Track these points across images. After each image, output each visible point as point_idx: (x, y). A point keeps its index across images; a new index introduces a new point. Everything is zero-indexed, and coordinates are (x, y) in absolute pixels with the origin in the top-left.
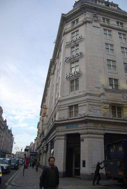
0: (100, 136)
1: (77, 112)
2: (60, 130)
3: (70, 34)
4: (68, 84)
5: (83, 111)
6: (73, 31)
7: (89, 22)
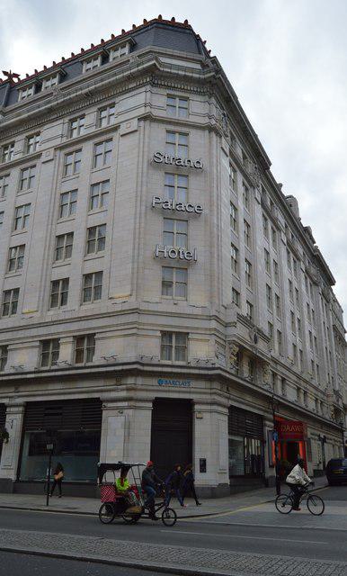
1: (182, 350)
2: (140, 387)
3: (90, 145)
4: (154, 275)
5: (201, 351)
6: (97, 140)
7: (218, 133)
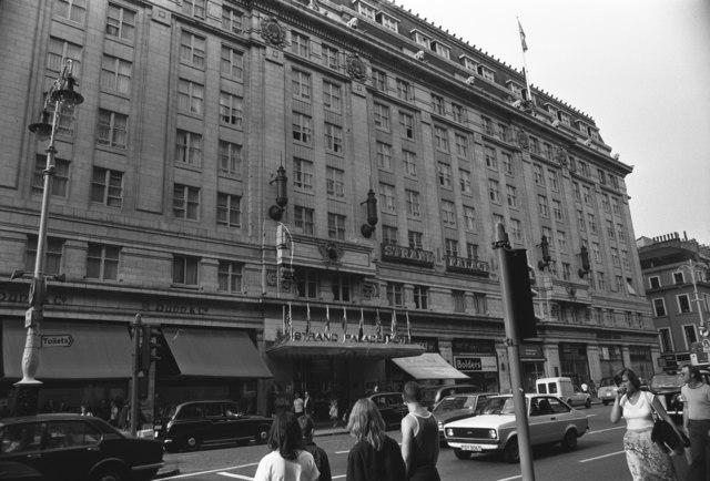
7: (258, 46)
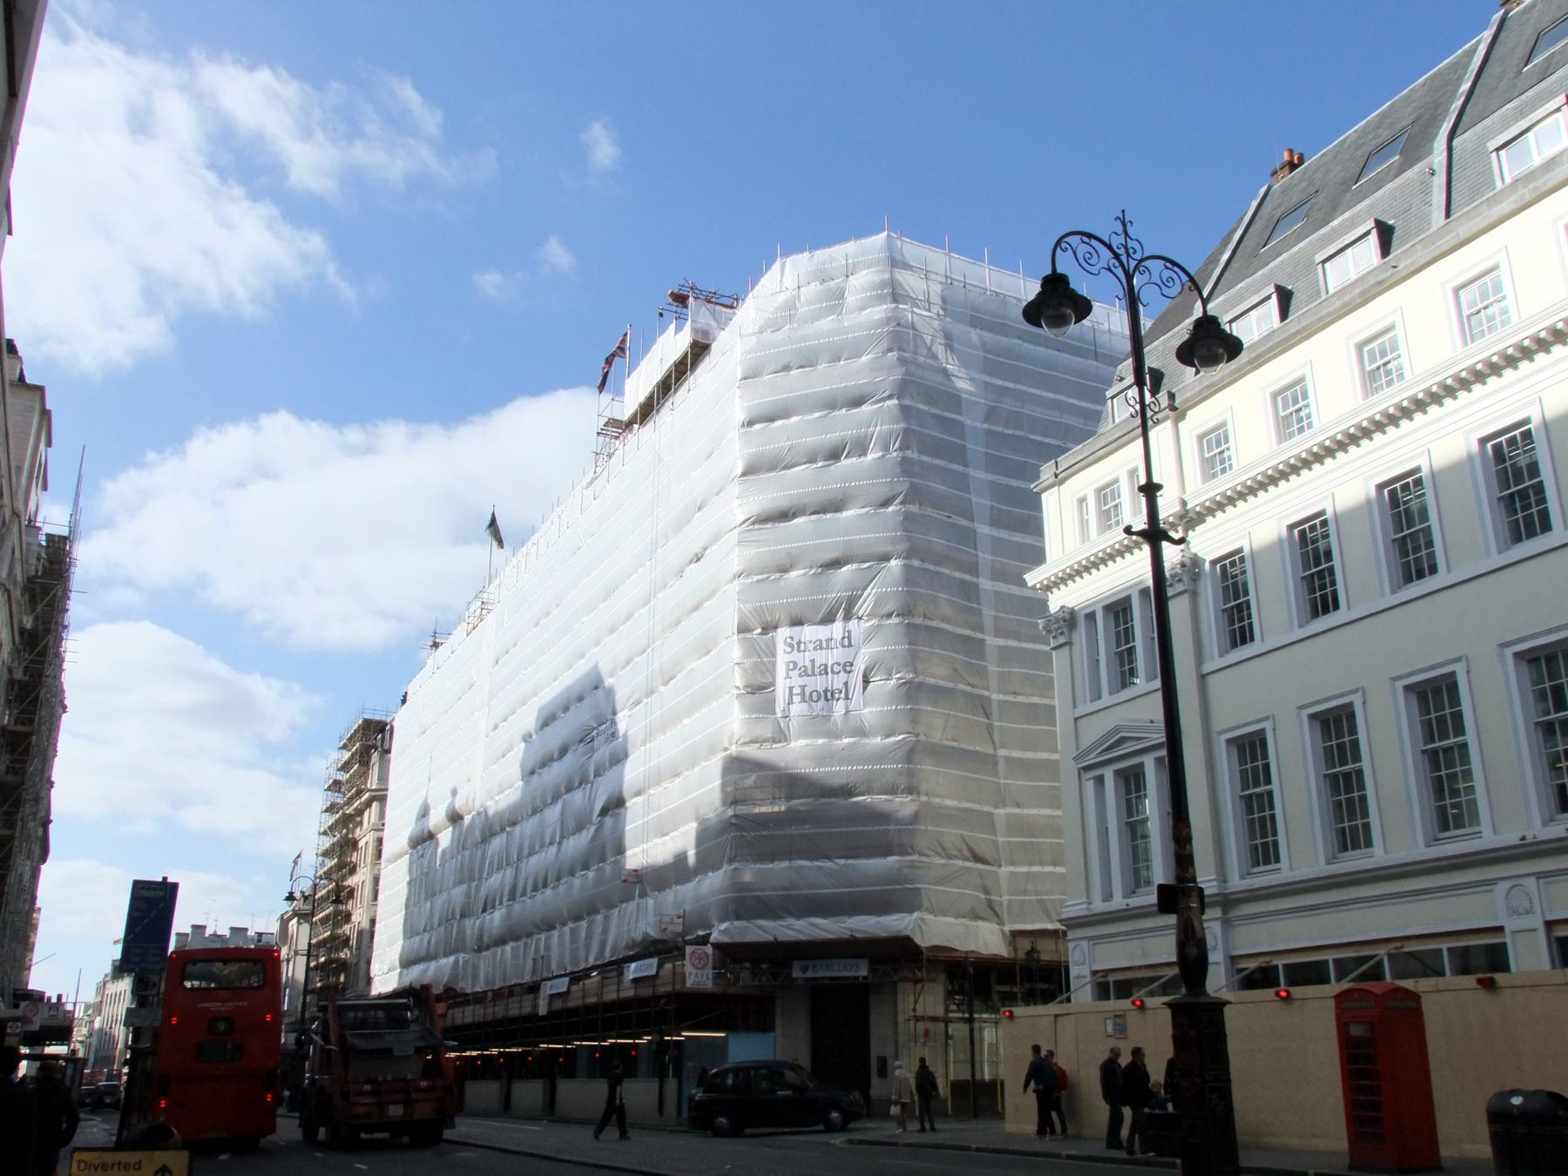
0: (1170, 931)
